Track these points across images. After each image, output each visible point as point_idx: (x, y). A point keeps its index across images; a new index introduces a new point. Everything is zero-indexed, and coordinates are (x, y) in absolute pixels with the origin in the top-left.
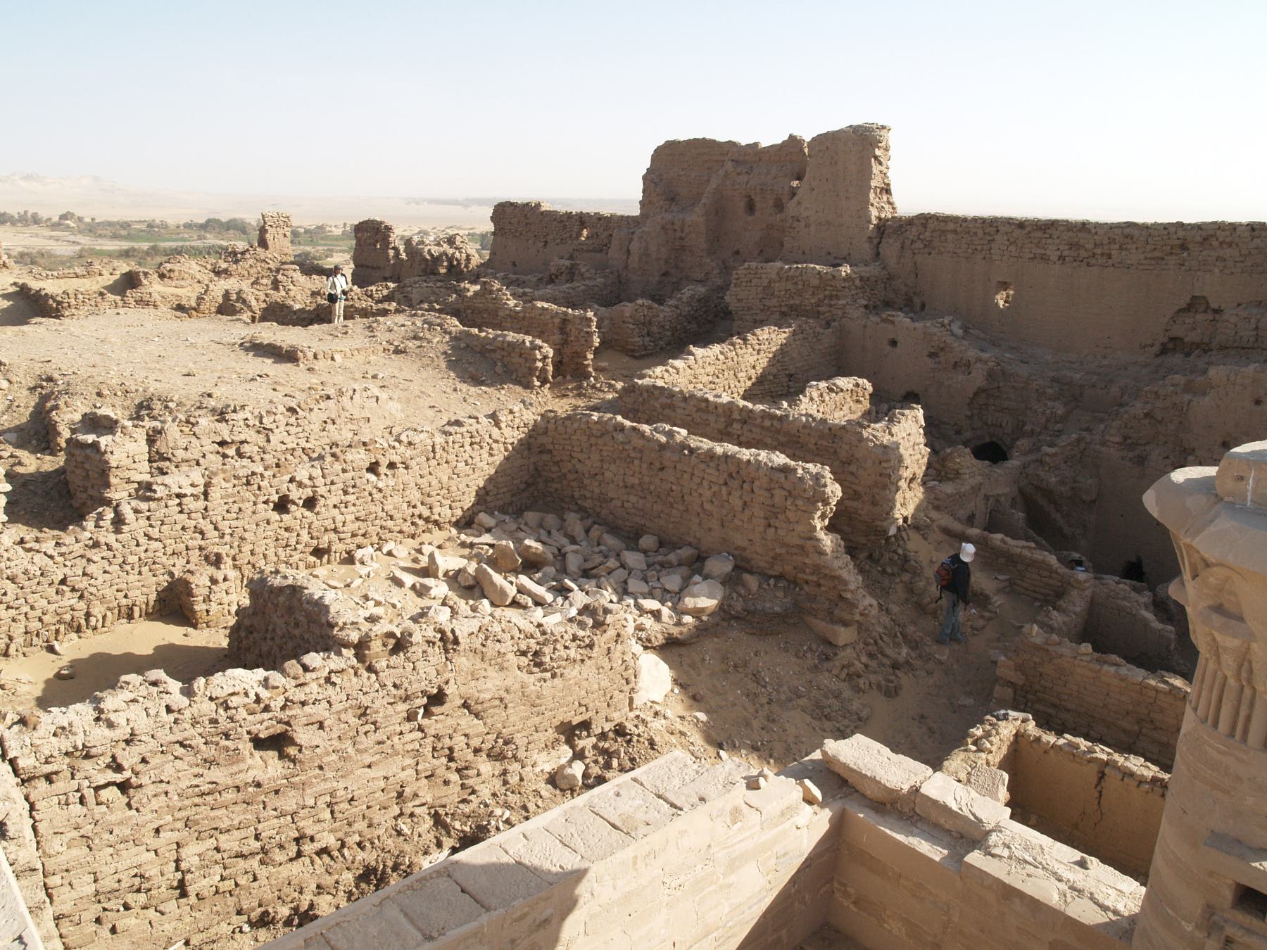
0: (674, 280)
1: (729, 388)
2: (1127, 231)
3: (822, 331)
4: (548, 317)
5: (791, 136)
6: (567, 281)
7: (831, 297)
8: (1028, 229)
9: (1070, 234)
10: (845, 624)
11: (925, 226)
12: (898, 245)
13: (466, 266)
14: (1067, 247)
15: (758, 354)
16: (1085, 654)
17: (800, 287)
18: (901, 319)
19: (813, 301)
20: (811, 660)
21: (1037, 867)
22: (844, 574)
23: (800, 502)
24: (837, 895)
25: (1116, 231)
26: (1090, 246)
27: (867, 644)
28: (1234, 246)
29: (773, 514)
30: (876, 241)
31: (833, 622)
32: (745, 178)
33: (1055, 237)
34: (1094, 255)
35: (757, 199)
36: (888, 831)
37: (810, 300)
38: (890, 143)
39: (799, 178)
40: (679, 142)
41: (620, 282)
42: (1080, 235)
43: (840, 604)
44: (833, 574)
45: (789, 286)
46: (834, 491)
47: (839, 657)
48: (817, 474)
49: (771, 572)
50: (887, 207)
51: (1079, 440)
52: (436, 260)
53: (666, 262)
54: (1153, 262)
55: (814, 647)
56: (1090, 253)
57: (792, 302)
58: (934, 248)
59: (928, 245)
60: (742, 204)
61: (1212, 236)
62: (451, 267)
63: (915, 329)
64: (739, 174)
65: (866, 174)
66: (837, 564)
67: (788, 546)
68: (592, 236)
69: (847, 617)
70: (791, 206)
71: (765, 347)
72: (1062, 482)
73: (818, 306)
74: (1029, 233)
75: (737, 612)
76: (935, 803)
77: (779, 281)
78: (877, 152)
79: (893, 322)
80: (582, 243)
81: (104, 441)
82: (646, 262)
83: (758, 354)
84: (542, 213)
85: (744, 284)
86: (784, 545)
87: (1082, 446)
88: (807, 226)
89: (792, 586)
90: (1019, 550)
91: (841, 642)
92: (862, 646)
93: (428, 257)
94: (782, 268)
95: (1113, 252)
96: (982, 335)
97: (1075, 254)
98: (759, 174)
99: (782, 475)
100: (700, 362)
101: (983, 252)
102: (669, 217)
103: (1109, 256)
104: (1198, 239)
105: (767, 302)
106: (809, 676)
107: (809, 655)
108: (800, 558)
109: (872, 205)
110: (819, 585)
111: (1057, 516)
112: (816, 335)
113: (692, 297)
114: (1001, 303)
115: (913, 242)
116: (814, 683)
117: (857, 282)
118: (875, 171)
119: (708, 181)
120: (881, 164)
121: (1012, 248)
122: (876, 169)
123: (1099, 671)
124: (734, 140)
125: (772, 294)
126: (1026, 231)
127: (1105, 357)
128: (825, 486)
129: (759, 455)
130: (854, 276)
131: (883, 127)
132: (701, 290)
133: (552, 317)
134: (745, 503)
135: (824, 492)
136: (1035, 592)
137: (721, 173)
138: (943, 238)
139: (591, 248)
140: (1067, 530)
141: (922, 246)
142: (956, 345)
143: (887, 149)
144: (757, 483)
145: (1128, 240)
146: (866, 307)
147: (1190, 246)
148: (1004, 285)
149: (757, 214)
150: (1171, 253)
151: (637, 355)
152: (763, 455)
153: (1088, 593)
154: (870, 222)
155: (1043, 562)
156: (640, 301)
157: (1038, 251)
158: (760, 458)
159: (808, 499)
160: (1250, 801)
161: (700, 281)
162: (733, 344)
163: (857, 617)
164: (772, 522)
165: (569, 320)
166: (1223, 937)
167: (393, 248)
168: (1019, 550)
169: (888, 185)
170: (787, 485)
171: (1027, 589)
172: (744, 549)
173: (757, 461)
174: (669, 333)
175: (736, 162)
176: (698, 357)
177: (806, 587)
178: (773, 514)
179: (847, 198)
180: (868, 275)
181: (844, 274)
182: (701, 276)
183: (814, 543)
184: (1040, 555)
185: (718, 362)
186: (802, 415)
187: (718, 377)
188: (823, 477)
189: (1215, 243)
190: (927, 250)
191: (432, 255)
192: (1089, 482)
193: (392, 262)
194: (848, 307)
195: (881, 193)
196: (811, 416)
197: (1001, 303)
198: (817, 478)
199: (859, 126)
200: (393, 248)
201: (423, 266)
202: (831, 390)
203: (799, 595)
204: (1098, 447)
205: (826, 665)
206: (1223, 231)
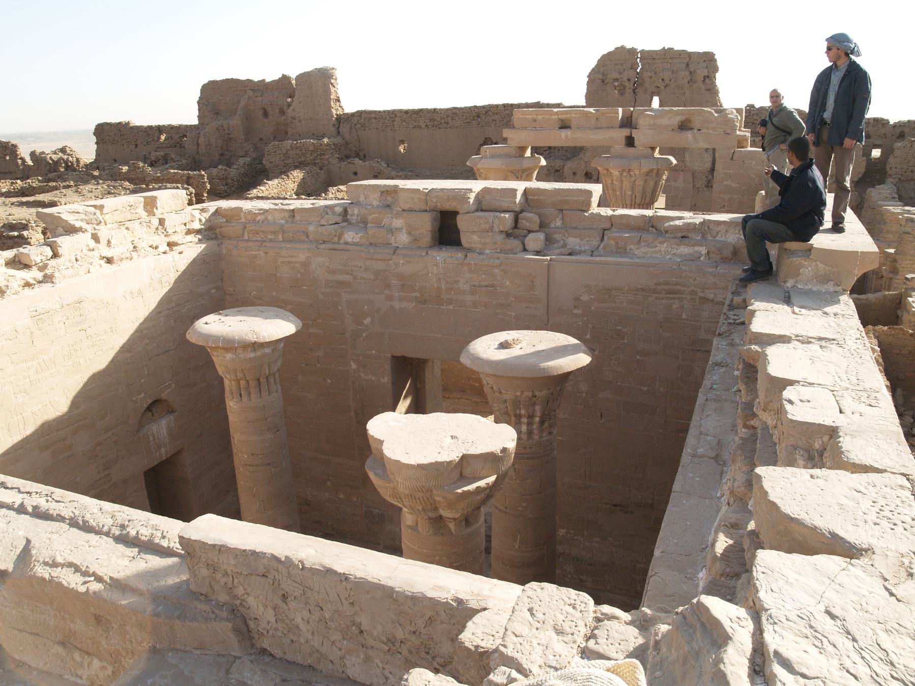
0: (228, 157)
2: (454, 111)
4: (179, 177)
5: (827, 40)
6: (163, 164)
9: (429, 114)
11: (360, 116)
12: (348, 127)
13: (78, 165)
18: (357, 161)
19: (311, 158)
30: (337, 126)
32: (260, 99)
34: (441, 123)
35: (269, 109)
38: (337, 77)
40: (217, 81)
41: (195, 162)
45: (298, 152)
50: (339, 108)
52: (57, 163)
53: (221, 148)
56: (439, 123)
57: (300, 160)
59: (363, 126)
60: (261, 113)
62: (67, 167)
63: (365, 165)
64: (256, 97)
65: (328, 93)
68: (168, 139)
74: (411, 115)
78: (332, 81)
79: (354, 164)
80: (161, 143)
81: (25, 233)
82: (210, 149)
84: (132, 127)
93: (51, 162)
94: (293, 143)
95: (449, 121)
96: (396, 167)
97: (433, 123)
100: (271, 187)
102: (220, 123)
103: (448, 123)
105: (286, 162)
112: (317, 174)
113: (244, 163)
114: (402, 150)
115: (355, 125)
117: (333, 146)
118: (332, 91)
121: (404, 123)
122: (332, 89)
125: (289, 157)
126: (409, 115)
127: (452, 170)
131: (333, 69)
132: (248, 160)
133: (181, 177)
137: (246, 97)
138: (370, 122)
139: (169, 145)
142: (385, 170)
143: (336, 80)
146: (338, 158)
147: (481, 116)
148: (402, 142)
151: (222, 195)
154: (333, 116)
156: (220, 167)
157: (416, 124)
162: (283, 179)
165: (191, 177)
167: (20, 158)
169: (339, 97)
174: (236, 183)
176: (270, 185)
180: (337, 142)
189: (491, 114)
190: (363, 128)
191: (53, 160)
193: (21, 167)
197: (402, 150)
199: (321, 69)
200: (20, 158)
201: (48, 168)
202: (338, 191)
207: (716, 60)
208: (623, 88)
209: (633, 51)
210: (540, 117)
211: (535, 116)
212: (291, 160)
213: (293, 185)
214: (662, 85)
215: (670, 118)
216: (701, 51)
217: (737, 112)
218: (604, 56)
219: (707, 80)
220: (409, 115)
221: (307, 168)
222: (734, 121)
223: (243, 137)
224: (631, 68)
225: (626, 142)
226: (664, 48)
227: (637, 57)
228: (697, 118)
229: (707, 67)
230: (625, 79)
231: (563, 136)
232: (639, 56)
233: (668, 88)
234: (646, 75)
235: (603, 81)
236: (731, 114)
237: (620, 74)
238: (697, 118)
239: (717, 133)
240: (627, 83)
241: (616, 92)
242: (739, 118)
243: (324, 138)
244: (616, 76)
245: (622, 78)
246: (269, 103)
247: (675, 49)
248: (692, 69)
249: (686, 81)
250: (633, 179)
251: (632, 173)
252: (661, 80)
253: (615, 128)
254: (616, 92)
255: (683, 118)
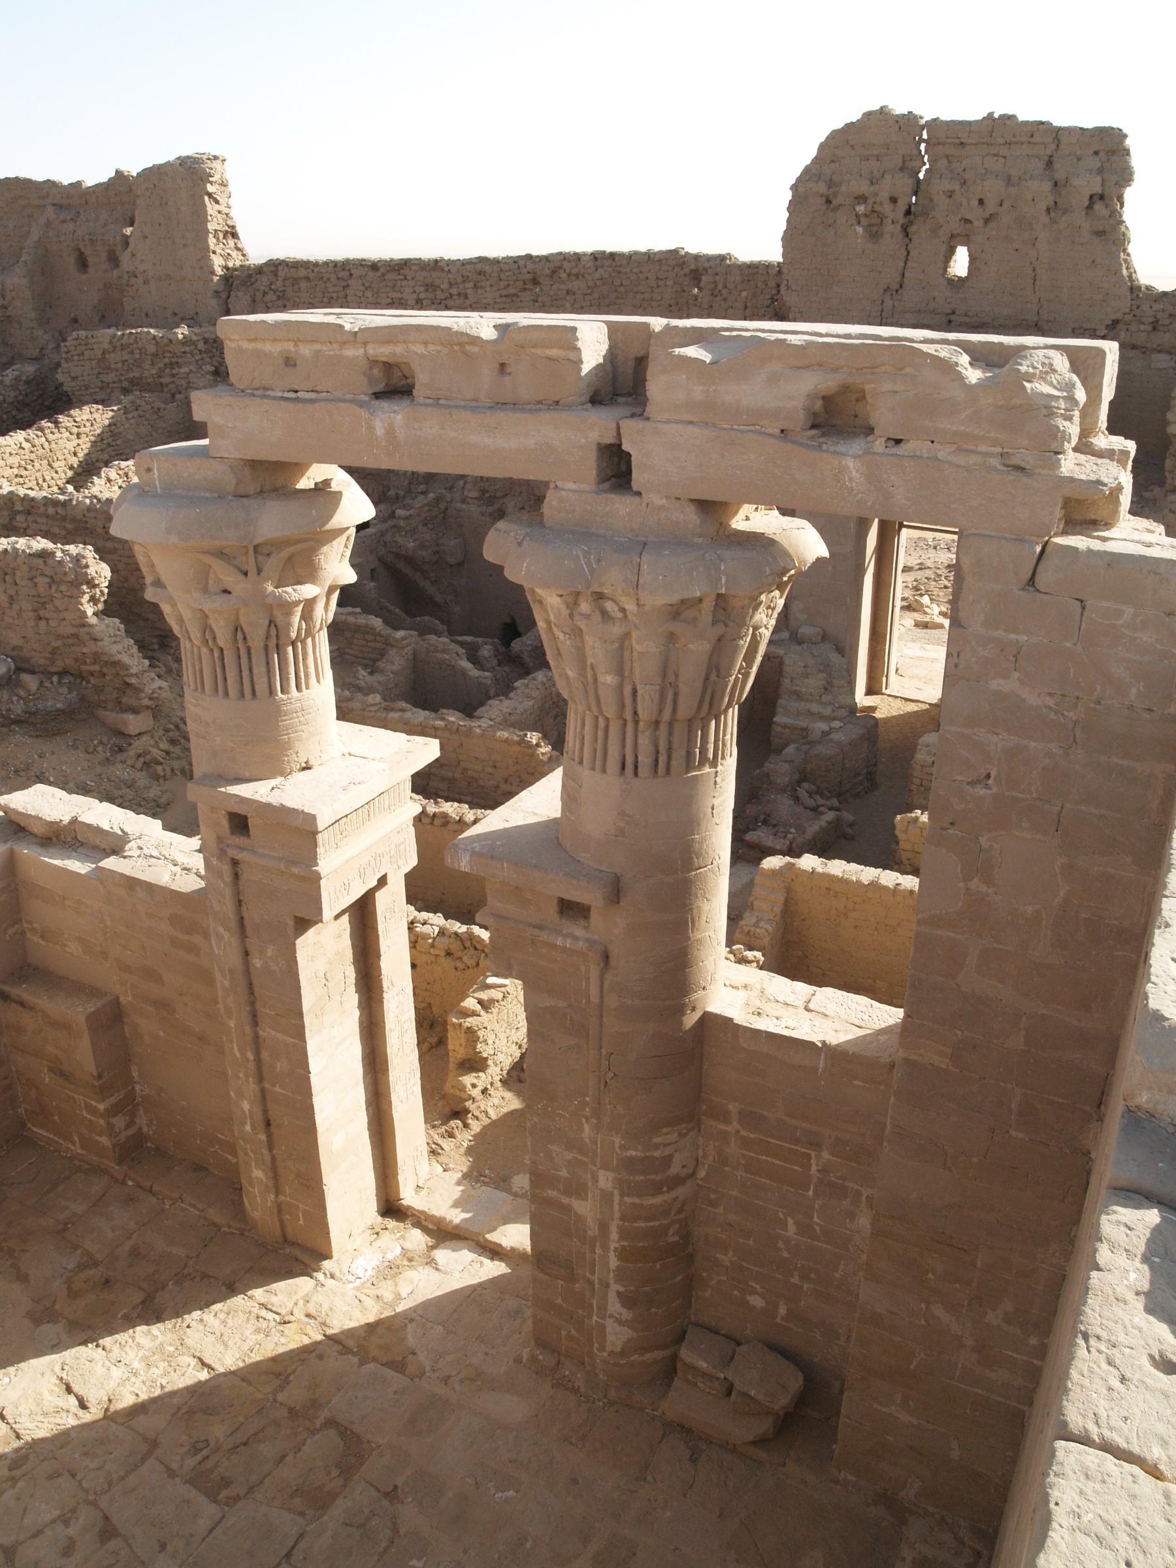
1: (44, 480)
2: (479, 267)
3: (162, 405)
7: (171, 365)
8: (382, 270)
9: (424, 274)
10: (135, 711)
11: (275, 273)
14: (423, 289)
15: (78, 438)
16: (372, 705)
17: (137, 356)
19: (154, 372)
20: (103, 753)
21: (159, 859)
22: (126, 659)
23: (63, 588)
24: (29, 935)
25: (468, 267)
26: (445, 286)
27: (167, 731)
28: (581, 277)
29: (41, 603)
30: (224, 295)
31: (123, 711)
32: (71, 226)
33: (409, 278)
34: (451, 295)
35: (88, 251)
36: (47, 859)
37: (149, 371)
39: (132, 225)
42: (435, 274)
43: (128, 692)
44: (113, 659)
45: (126, 356)
46: (101, 572)
47: (133, 746)
48: (77, 555)
49: (53, 669)
50: (234, 254)
51: (438, 500)
54: (508, 300)
55: (105, 740)
57: (131, 375)
58: (289, 300)
60: (72, 260)
61: (560, 267)
64: (63, 222)
65: (201, 217)
66: (115, 649)
67: (63, 637)
69: (134, 702)
70: (125, 257)
71: (87, 430)
72: (423, 547)
73: (160, 377)
74: (383, 275)
75: (18, 715)
76: (89, 826)
77: (114, 351)
78: (210, 188)
83: (78, 438)
85: (76, 358)
86: (59, 637)
87: (442, 506)
88: (146, 282)
89: (78, 680)
90: (344, 617)
91: (133, 729)
92: (161, 732)
94: (114, 336)
95: (469, 291)
98: (87, 220)
99: (40, 561)
101: (340, 300)
103: (466, 296)
104: (547, 272)
106: (99, 770)
107: (100, 749)
108: (78, 649)
109: (214, 252)
110: (104, 675)
111: (424, 584)
113: (17, 379)
115: (265, 294)
116: (103, 776)
117: (201, 345)
119: (28, 232)
120: (217, 202)
121: (368, 294)
122: (211, 209)
123: (385, 718)
124: (53, 178)
125: (109, 368)
126: (379, 273)
128: (87, 566)
129: (17, 543)
130: (195, 338)
131: (216, 158)
132: (30, 369)
134: (11, 598)
135: (86, 573)
136: (364, 658)
137: (42, 221)
138: (296, 287)
140: (439, 598)
141: (274, 298)
144: (18, 573)
145: (482, 277)
147: (541, 280)
149: (91, 270)
150: (525, 289)
152: (22, 543)
153: (409, 650)
154: (213, 273)
155: (367, 626)
158: (18, 546)
159: (71, 582)
160: (218, 740)
161: (35, 359)
162: (41, 429)
163: (146, 702)
164: (42, 613)
166: (229, 859)
168: (344, 617)
169: (233, 227)
170: (48, 571)
171: (357, 657)
172: (21, 648)
173: (15, 550)
175: (59, 207)
177: (93, 680)
178: (41, 603)
179: (185, 245)
181: (180, 336)
182: (36, 353)
183: (86, 629)
184: (362, 620)
185: (22, 452)
186: (87, 497)
187: (26, 469)
188: (84, 557)
189: (563, 276)
192: (452, 543)
194: (191, 375)
195: (224, 237)
196: (96, 497)
198: (77, 559)
199: (188, 157)
203: (86, 688)
204: (458, 505)
205: (119, 757)
206: (569, 261)
207: (1127, 152)
208: (878, 221)
209: (909, 122)
210: (306, 350)
211: (290, 346)
212: (113, 375)
213: (76, 442)
214: (975, 214)
215: (773, 379)
216: (1089, 124)
217: (1074, 368)
218: (834, 135)
219: (1099, 207)
220: (379, 273)
221: (126, 400)
222: (1051, 414)
223: (32, 315)
224: (902, 169)
225: (600, 470)
226: (991, 115)
227: (921, 140)
228: (887, 386)
229: (1100, 171)
230: (884, 195)
231: (380, 429)
232: (925, 136)
233: (993, 224)
234: (940, 187)
235: (828, 202)
236: (1043, 377)
237: (872, 184)
238: (887, 386)
239: (973, 459)
240: (887, 208)
241: (860, 230)
242: (1081, 395)
243: (178, 327)
244: (864, 187)
245: (876, 195)
246: (87, 238)
247: (1021, 118)
248: (1060, 175)
249: (1043, 206)
250: (617, 630)
251: (609, 606)
252: (975, 203)
253: (569, 407)
254: (860, 230)
255: (828, 383)
